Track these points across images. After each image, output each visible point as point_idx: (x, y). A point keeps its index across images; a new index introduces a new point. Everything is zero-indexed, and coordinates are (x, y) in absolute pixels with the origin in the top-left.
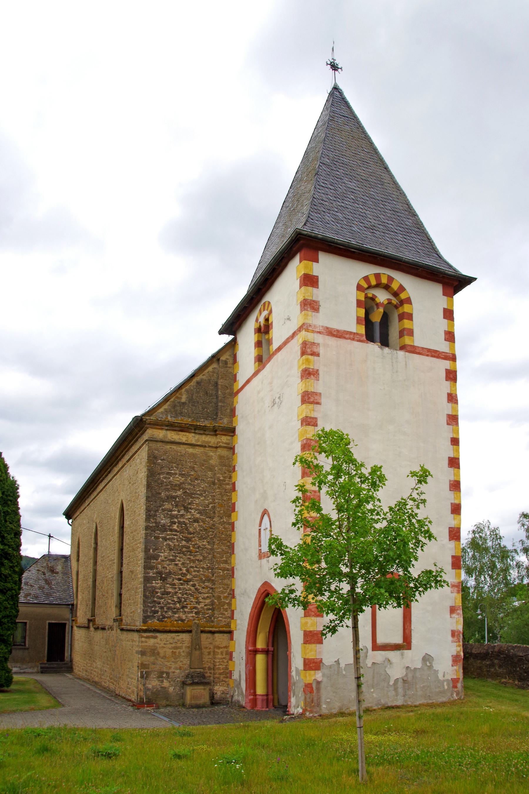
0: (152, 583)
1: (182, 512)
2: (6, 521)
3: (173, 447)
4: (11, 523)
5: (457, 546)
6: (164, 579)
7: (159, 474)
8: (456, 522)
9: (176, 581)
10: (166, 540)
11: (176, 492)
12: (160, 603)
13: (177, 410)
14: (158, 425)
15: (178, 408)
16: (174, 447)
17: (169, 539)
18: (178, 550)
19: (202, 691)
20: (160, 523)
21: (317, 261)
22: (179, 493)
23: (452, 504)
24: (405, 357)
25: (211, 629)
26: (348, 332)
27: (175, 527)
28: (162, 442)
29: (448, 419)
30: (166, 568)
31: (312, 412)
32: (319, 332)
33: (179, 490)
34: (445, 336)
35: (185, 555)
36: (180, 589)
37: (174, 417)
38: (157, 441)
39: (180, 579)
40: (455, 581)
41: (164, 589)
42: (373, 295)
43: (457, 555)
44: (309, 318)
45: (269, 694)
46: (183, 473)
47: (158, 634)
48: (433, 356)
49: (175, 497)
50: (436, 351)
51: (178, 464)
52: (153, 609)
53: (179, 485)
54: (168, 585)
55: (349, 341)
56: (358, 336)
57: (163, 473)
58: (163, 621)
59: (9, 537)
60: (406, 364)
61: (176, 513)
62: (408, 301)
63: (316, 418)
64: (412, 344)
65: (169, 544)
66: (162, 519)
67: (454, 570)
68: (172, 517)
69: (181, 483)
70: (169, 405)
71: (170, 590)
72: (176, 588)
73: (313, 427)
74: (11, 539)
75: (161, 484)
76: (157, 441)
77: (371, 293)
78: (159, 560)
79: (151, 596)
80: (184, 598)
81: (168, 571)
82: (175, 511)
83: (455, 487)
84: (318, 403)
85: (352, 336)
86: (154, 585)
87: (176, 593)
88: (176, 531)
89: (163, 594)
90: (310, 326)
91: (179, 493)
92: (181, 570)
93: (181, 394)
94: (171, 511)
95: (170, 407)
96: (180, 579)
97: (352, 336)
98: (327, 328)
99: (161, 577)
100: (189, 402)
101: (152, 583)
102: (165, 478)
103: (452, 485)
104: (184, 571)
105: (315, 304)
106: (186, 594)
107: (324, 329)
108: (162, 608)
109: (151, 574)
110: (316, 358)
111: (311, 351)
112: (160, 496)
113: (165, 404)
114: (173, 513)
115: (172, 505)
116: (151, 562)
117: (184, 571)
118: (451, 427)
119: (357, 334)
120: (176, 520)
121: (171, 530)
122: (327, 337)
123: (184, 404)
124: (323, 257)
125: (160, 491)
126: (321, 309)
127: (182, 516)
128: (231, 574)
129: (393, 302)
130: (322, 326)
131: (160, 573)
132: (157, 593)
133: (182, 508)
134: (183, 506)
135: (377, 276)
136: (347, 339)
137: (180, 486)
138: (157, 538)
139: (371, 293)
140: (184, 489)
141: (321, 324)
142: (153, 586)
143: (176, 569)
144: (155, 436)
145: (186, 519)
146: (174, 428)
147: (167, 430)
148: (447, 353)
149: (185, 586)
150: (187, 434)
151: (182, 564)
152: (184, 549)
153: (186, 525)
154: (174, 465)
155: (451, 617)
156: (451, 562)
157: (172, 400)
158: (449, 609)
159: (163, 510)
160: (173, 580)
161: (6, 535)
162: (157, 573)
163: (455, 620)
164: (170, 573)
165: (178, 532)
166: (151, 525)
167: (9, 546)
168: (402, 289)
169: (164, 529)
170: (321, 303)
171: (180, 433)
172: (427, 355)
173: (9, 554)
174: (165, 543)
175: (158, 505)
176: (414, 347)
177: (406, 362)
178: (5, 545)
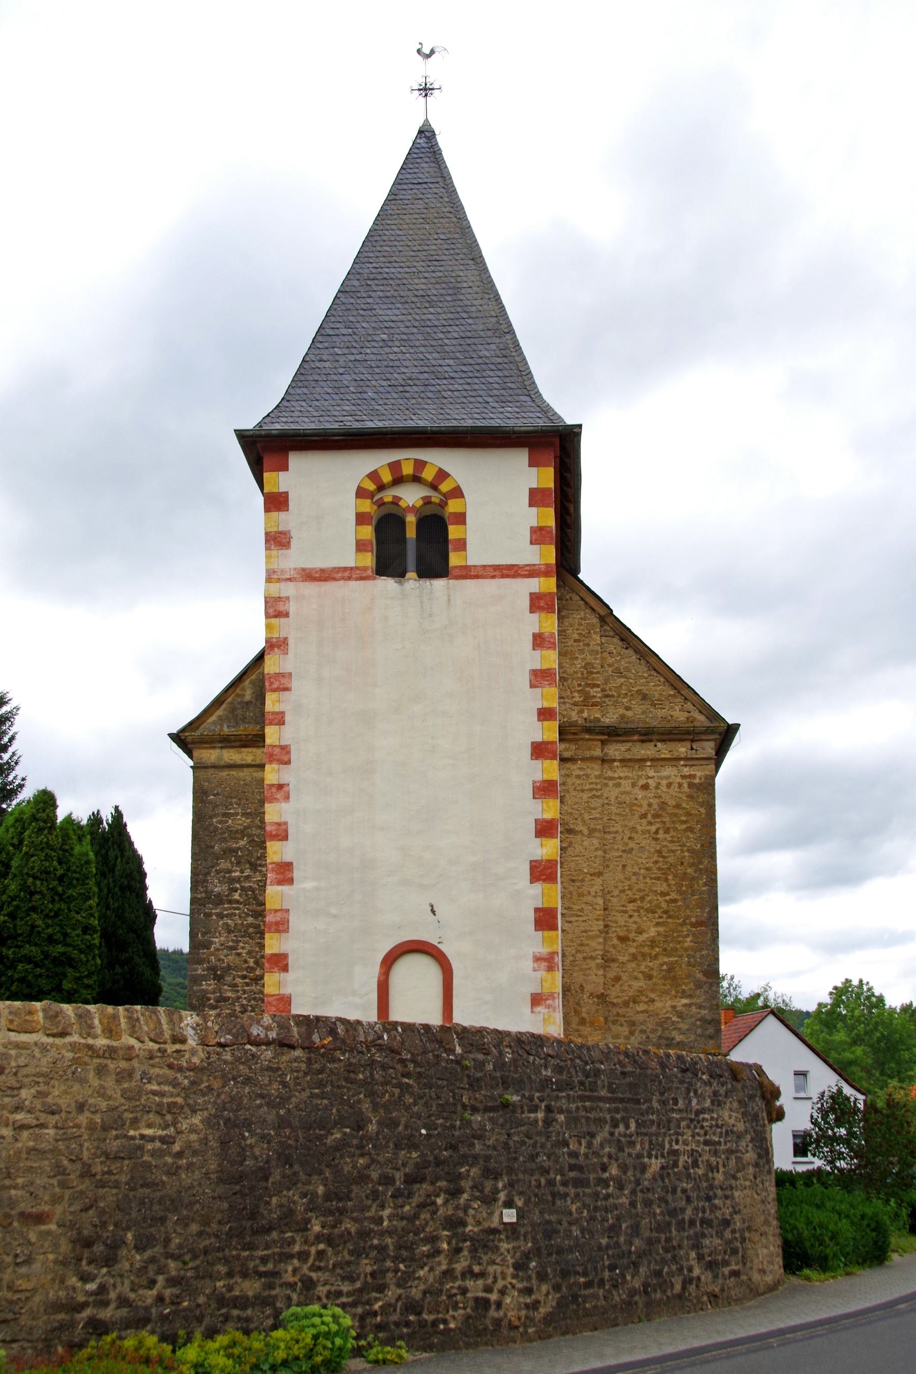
0: (202, 985)
1: (247, 872)
2: (70, 910)
3: (232, 773)
4: (78, 913)
5: (545, 891)
6: (219, 978)
7: (211, 817)
8: (545, 851)
9: (239, 981)
10: (222, 918)
11: (237, 843)
13: (237, 715)
14: (206, 743)
15: (239, 712)
16: (234, 773)
17: (227, 916)
18: (240, 931)
20: (212, 891)
21: (285, 468)
22: (242, 843)
23: (536, 821)
24: (448, 588)
26: (339, 568)
27: (236, 896)
28: (215, 767)
29: (533, 678)
30: (223, 960)
31: (277, 704)
32: (290, 580)
33: (242, 839)
34: (531, 537)
35: (252, 939)
36: (244, 992)
37: (234, 727)
38: (206, 767)
39: (244, 977)
40: (541, 950)
41: (220, 993)
42: (394, 497)
43: (546, 905)
44: (273, 560)
46: (249, 811)
48: (503, 576)
49: (235, 851)
50: (510, 567)
51: (240, 799)
53: (242, 832)
54: (226, 987)
55: (342, 582)
56: (358, 572)
57: (216, 815)
59: (74, 934)
60: (449, 600)
61: (237, 874)
62: (457, 492)
63: (283, 713)
64: (464, 564)
65: (227, 924)
66: (216, 886)
67: (540, 933)
68: (233, 880)
69: (246, 828)
70: (225, 710)
71: (229, 994)
72: (238, 991)
73: (277, 727)
74: (78, 936)
75: (215, 831)
76: (206, 767)
77: (388, 496)
78: (212, 949)
79: (200, 1005)
80: (251, 1006)
81: (225, 965)
82: (235, 871)
83: (544, 791)
84: (287, 689)
85: (347, 574)
86: (204, 987)
87: (239, 998)
88: (238, 902)
89: (218, 1001)
90: (274, 572)
91: (242, 843)
92: (246, 962)
93: (244, 689)
94: (230, 872)
95: (226, 713)
96: (244, 977)
97: (347, 574)
98: (303, 570)
99: (215, 974)
100: (257, 700)
101: (202, 985)
102: (220, 822)
103: (538, 788)
104: (252, 964)
105: (283, 536)
106: (255, 999)
107: (298, 573)
109: (199, 972)
110: (283, 620)
111: (275, 611)
112: (211, 850)
113: (218, 709)
114: (233, 874)
115: (231, 862)
116: (199, 954)
117: (252, 964)
118: (538, 690)
119: (357, 568)
120: (238, 886)
121: (230, 902)
122: (302, 584)
123: (248, 703)
124: (296, 460)
125: (213, 844)
126: (293, 543)
127: (248, 878)
129: (433, 500)
130: (295, 569)
131: (213, 969)
132: (209, 999)
133: (248, 866)
134: (249, 862)
135: (395, 467)
136: (338, 580)
137: (243, 833)
138: (208, 915)
139: (388, 496)
140: (249, 836)
141: (292, 566)
143: (237, 961)
144: (203, 760)
145: (254, 882)
146: (233, 744)
147: (222, 748)
148: (534, 565)
149: (253, 988)
150: (254, 750)
151: (247, 954)
152: (251, 930)
153: (253, 892)
154: (234, 800)
155: (532, 1012)
156: (533, 919)
157: (229, 700)
158: (529, 998)
159: (218, 872)
160: (234, 979)
161: (69, 931)
162: (208, 969)
163: (541, 1017)
164: (229, 967)
165: (241, 903)
166: (199, 896)
167: (74, 947)
168: (442, 475)
169: (219, 900)
170: (292, 534)
171: (243, 750)
172: (493, 577)
173: (74, 959)
174: (221, 923)
175: (210, 864)
176: (466, 567)
177: (449, 596)
178: (70, 945)
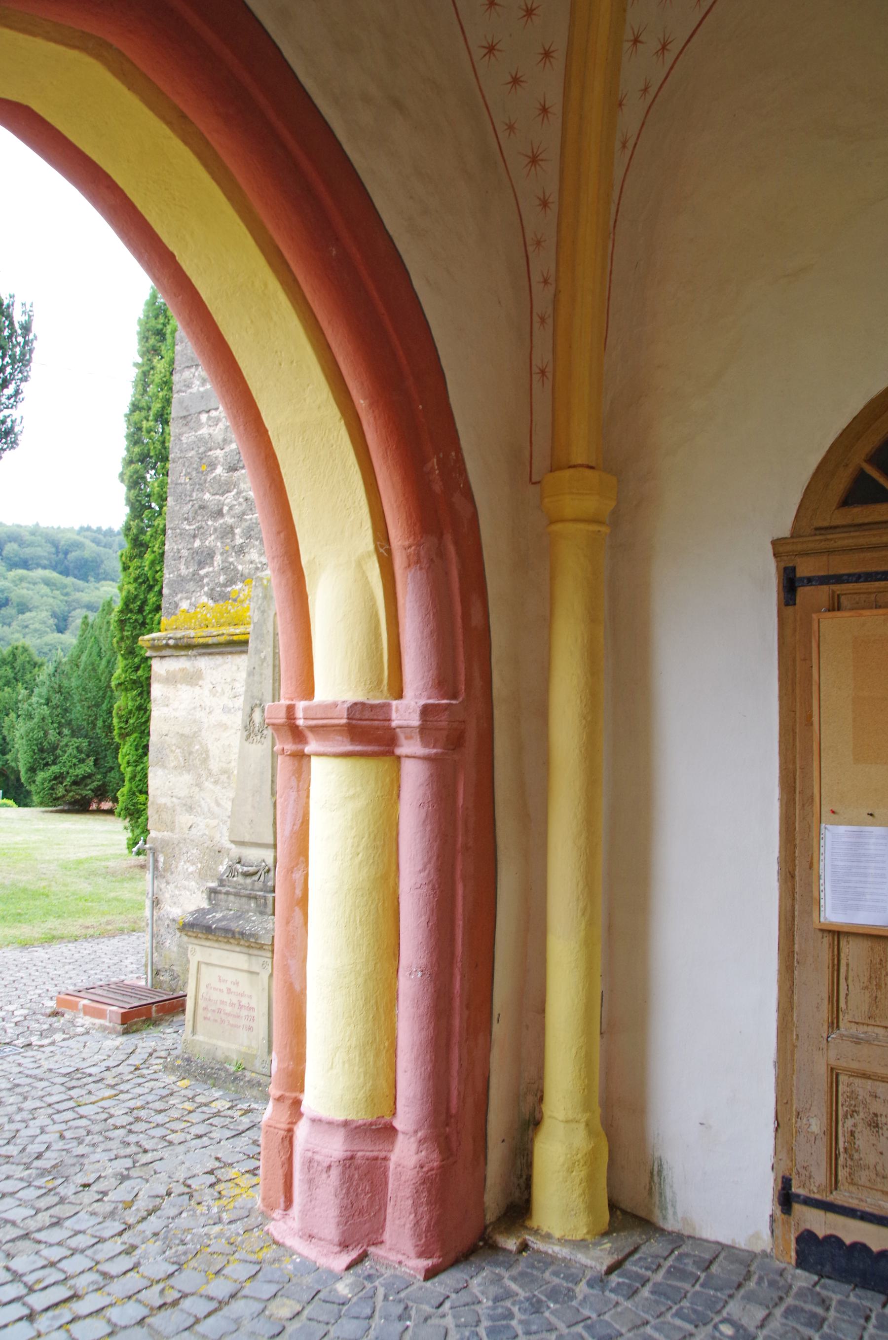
0: (200, 425)
12: (220, 513)
19: (243, 978)
25: (232, 630)
45: (398, 1124)
47: (204, 663)
52: (197, 543)
58: (225, 597)
86: (204, 431)
108: (229, 531)
128: (135, 407)
142: (201, 439)
